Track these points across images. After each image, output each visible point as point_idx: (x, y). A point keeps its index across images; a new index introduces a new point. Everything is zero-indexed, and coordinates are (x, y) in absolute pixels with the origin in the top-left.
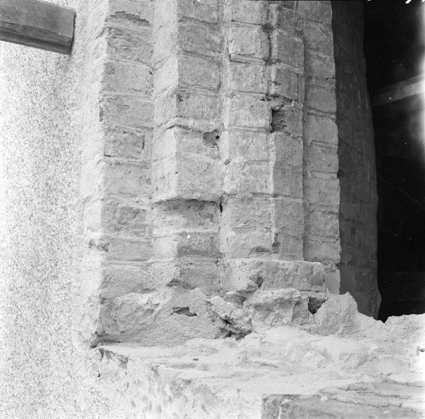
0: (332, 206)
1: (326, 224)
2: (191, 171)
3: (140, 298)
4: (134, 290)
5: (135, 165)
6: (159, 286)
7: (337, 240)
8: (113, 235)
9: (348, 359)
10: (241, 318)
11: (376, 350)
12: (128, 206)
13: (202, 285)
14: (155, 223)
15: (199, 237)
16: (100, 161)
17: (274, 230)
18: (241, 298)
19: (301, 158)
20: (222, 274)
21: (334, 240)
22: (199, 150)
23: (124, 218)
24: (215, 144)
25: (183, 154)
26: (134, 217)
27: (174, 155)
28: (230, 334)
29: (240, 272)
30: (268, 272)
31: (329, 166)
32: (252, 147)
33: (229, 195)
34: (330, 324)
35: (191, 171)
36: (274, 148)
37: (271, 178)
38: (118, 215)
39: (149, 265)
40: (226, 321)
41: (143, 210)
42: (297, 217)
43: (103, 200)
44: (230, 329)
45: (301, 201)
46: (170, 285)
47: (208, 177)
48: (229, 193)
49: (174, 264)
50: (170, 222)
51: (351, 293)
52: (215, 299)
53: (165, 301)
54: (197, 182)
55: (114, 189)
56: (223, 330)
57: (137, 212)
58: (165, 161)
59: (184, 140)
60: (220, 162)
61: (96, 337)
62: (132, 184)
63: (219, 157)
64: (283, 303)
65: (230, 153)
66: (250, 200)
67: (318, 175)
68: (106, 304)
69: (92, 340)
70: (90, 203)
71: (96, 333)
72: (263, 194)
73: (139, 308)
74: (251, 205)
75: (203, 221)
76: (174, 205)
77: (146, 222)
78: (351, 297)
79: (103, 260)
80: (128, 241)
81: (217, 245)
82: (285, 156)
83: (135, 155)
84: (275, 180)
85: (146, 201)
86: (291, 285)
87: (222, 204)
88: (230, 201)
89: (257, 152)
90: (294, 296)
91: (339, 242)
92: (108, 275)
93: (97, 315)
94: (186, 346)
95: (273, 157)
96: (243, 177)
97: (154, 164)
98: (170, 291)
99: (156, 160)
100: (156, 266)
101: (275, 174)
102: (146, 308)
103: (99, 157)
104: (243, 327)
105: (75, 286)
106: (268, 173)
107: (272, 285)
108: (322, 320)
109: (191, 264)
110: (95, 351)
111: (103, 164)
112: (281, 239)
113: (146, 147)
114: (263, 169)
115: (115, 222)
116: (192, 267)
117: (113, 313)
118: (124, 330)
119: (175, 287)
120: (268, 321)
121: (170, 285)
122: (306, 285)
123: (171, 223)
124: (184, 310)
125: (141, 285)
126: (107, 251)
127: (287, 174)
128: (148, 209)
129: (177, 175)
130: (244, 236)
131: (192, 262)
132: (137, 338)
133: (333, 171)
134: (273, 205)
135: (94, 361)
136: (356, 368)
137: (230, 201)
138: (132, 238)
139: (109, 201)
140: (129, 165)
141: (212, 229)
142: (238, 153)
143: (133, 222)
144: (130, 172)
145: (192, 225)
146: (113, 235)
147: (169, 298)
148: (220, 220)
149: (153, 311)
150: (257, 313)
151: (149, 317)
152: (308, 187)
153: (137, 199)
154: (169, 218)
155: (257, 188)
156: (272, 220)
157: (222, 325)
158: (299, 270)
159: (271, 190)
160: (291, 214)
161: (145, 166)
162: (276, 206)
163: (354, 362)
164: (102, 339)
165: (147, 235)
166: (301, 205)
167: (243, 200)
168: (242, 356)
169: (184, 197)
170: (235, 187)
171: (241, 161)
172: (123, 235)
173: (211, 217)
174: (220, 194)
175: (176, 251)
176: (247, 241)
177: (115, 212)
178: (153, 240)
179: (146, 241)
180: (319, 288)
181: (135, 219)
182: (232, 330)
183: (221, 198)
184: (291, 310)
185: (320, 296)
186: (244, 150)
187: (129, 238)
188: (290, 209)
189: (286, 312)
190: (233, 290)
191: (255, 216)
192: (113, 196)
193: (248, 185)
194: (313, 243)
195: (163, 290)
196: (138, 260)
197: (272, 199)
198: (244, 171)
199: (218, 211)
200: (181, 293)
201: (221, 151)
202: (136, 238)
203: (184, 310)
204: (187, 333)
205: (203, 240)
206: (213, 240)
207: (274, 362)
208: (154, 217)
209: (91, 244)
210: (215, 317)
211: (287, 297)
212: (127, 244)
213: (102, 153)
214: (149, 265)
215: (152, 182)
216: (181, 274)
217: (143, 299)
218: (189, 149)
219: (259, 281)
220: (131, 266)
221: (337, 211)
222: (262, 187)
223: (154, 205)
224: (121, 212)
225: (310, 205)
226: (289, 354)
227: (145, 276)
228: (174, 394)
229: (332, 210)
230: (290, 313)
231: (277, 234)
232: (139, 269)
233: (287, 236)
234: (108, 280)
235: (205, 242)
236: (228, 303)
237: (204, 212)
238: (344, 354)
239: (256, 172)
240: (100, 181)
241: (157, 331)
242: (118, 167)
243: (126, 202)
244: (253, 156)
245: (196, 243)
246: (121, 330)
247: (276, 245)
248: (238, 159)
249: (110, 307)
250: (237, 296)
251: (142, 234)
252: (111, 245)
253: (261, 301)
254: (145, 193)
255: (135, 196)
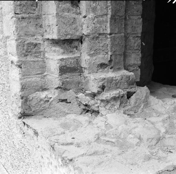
0: (138, 33)
1: (135, 43)
2: (64, 23)
3: (41, 94)
4: (38, 90)
5: (33, 18)
6: (52, 88)
7: (140, 50)
8: (23, 59)
9: (151, 141)
10: (94, 105)
11: (164, 133)
12: (30, 42)
13: (73, 88)
14: (46, 50)
15: (70, 60)
16: (12, 17)
17: (110, 53)
18: (94, 95)
19: (124, 10)
20: (83, 81)
21: (138, 51)
22: (69, 11)
23: (29, 49)
24: (78, 6)
25: (60, 14)
26: (35, 48)
27: (55, 14)
28: (88, 111)
29: (93, 84)
30: (108, 83)
31: (138, 11)
32: (99, 7)
33: (86, 36)
34: (137, 104)
35: (64, 23)
36: (110, 7)
37: (108, 25)
38: (25, 48)
39: (45, 76)
40: (86, 105)
41: (39, 43)
42: (121, 43)
43: (16, 40)
44: (87, 109)
45: (123, 34)
46: (57, 88)
47: (74, 26)
48: (86, 34)
49: (58, 79)
50: (54, 50)
51: (147, 86)
52: (80, 95)
53: (55, 96)
54: (68, 30)
55: (22, 33)
56: (84, 110)
57: (36, 45)
58: (50, 16)
59: (60, 6)
60: (81, 17)
61: (20, 115)
62: (32, 29)
63: (80, 14)
64: (115, 99)
65: (86, 11)
66: (98, 38)
67: (131, 17)
68: (24, 99)
69: (19, 115)
70: (9, 40)
71: (20, 113)
72: (104, 34)
73: (41, 100)
74: (98, 41)
75: (72, 50)
76: (55, 42)
77: (41, 50)
78: (147, 88)
79: (20, 77)
80: (32, 61)
81: (80, 63)
82: (116, 11)
83: (32, 12)
84: (111, 25)
85: (40, 38)
86: (119, 88)
87: (82, 40)
88: (87, 39)
89: (102, 10)
90: (121, 94)
91: (140, 51)
92: (24, 85)
93: (20, 105)
94: (66, 118)
95: (110, 12)
96: (94, 25)
97: (43, 16)
98: (57, 91)
99: (45, 14)
100: (48, 77)
101: (111, 22)
102: (45, 100)
103: (12, 14)
104: (95, 109)
105: (7, 86)
106: (107, 22)
107: (110, 89)
108: (133, 103)
109: (67, 78)
110: (20, 121)
111: (14, 19)
112: (113, 58)
113: (38, 7)
114: (104, 20)
115: (24, 52)
116: (68, 80)
117: (28, 103)
118: (34, 110)
119: (60, 90)
120: (107, 107)
121: (57, 88)
122: (126, 86)
123: (55, 51)
124: (65, 101)
125: (41, 87)
126: (21, 68)
127: (117, 21)
128: (42, 42)
129: (57, 26)
130: (94, 58)
131: (68, 77)
132: (42, 113)
133: (139, 14)
134: (109, 40)
135: (21, 126)
136: (155, 145)
137: (87, 39)
138: (34, 59)
139: (20, 41)
140: (29, 18)
141: (77, 55)
142: (91, 12)
143: (34, 50)
144: (30, 22)
145: (66, 53)
146: (23, 59)
147: (56, 94)
148: (81, 49)
149: (48, 101)
150: (102, 103)
151: (47, 104)
152: (127, 24)
153: (35, 37)
154: (54, 48)
155: (101, 31)
156: (108, 48)
157: (84, 107)
158: (123, 79)
159: (109, 31)
160: (118, 43)
161: (38, 17)
162: (111, 40)
163: (154, 142)
164: (24, 115)
165: (42, 56)
166: (123, 37)
167: (93, 38)
168: (97, 137)
169: (62, 39)
170: (89, 31)
171: (92, 16)
172: (29, 58)
173: (76, 47)
174: (81, 35)
175: (59, 69)
176: (96, 61)
177: (24, 46)
178: (45, 59)
179: (42, 60)
180: (132, 86)
181: (35, 49)
182: (89, 109)
183: (82, 37)
184: (119, 101)
185: (133, 90)
186: (94, 10)
187: (32, 59)
188: (118, 40)
189: (116, 102)
190: (89, 91)
191: (100, 46)
192: (22, 38)
193: (96, 30)
194: (128, 54)
195: (53, 91)
196: (39, 74)
197: (109, 36)
198: (94, 22)
199: (80, 43)
200: (63, 92)
201: (81, 9)
202: (36, 59)
203: (65, 101)
204: (67, 111)
205: (73, 61)
206: (78, 61)
207: (113, 140)
208: (45, 47)
209: (12, 62)
210: (80, 104)
211: (117, 96)
212: (32, 63)
213: (13, 12)
214: (45, 76)
215: (43, 26)
216: (62, 84)
217: (43, 95)
218: (63, 11)
219: (103, 88)
220: (36, 78)
221: (140, 35)
222: (103, 30)
223: (45, 40)
224: (27, 46)
225: (127, 34)
226: (120, 134)
227: (43, 82)
228: (64, 164)
229: (138, 35)
230: (119, 103)
231: (111, 56)
232: (39, 79)
233: (116, 55)
234: (24, 87)
235: (74, 62)
236: (87, 97)
237: (73, 45)
238: (149, 138)
239: (100, 22)
240: (14, 29)
241: (51, 110)
242: (23, 20)
243: (30, 40)
244: (99, 13)
245: (69, 63)
246: (33, 110)
247: (110, 61)
248: (91, 15)
249: (26, 101)
250: (91, 94)
251: (40, 56)
252: (23, 65)
253: (104, 99)
254: (39, 33)
255: (34, 36)
